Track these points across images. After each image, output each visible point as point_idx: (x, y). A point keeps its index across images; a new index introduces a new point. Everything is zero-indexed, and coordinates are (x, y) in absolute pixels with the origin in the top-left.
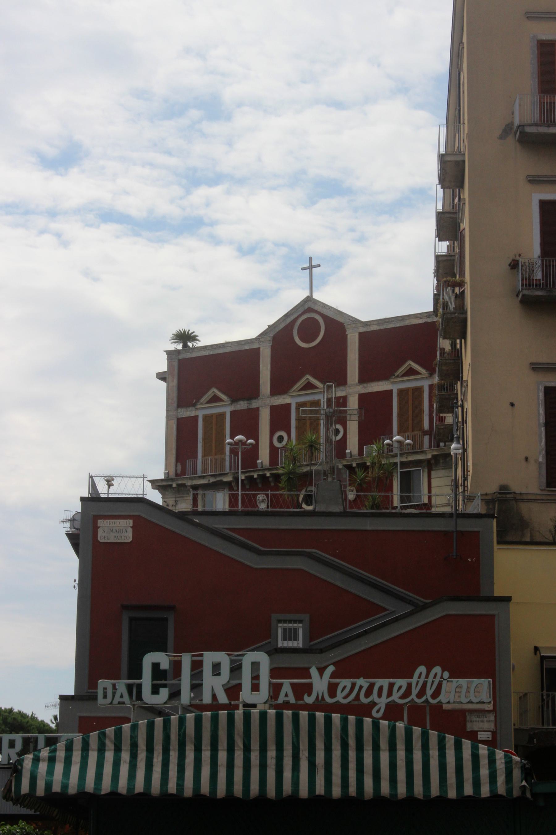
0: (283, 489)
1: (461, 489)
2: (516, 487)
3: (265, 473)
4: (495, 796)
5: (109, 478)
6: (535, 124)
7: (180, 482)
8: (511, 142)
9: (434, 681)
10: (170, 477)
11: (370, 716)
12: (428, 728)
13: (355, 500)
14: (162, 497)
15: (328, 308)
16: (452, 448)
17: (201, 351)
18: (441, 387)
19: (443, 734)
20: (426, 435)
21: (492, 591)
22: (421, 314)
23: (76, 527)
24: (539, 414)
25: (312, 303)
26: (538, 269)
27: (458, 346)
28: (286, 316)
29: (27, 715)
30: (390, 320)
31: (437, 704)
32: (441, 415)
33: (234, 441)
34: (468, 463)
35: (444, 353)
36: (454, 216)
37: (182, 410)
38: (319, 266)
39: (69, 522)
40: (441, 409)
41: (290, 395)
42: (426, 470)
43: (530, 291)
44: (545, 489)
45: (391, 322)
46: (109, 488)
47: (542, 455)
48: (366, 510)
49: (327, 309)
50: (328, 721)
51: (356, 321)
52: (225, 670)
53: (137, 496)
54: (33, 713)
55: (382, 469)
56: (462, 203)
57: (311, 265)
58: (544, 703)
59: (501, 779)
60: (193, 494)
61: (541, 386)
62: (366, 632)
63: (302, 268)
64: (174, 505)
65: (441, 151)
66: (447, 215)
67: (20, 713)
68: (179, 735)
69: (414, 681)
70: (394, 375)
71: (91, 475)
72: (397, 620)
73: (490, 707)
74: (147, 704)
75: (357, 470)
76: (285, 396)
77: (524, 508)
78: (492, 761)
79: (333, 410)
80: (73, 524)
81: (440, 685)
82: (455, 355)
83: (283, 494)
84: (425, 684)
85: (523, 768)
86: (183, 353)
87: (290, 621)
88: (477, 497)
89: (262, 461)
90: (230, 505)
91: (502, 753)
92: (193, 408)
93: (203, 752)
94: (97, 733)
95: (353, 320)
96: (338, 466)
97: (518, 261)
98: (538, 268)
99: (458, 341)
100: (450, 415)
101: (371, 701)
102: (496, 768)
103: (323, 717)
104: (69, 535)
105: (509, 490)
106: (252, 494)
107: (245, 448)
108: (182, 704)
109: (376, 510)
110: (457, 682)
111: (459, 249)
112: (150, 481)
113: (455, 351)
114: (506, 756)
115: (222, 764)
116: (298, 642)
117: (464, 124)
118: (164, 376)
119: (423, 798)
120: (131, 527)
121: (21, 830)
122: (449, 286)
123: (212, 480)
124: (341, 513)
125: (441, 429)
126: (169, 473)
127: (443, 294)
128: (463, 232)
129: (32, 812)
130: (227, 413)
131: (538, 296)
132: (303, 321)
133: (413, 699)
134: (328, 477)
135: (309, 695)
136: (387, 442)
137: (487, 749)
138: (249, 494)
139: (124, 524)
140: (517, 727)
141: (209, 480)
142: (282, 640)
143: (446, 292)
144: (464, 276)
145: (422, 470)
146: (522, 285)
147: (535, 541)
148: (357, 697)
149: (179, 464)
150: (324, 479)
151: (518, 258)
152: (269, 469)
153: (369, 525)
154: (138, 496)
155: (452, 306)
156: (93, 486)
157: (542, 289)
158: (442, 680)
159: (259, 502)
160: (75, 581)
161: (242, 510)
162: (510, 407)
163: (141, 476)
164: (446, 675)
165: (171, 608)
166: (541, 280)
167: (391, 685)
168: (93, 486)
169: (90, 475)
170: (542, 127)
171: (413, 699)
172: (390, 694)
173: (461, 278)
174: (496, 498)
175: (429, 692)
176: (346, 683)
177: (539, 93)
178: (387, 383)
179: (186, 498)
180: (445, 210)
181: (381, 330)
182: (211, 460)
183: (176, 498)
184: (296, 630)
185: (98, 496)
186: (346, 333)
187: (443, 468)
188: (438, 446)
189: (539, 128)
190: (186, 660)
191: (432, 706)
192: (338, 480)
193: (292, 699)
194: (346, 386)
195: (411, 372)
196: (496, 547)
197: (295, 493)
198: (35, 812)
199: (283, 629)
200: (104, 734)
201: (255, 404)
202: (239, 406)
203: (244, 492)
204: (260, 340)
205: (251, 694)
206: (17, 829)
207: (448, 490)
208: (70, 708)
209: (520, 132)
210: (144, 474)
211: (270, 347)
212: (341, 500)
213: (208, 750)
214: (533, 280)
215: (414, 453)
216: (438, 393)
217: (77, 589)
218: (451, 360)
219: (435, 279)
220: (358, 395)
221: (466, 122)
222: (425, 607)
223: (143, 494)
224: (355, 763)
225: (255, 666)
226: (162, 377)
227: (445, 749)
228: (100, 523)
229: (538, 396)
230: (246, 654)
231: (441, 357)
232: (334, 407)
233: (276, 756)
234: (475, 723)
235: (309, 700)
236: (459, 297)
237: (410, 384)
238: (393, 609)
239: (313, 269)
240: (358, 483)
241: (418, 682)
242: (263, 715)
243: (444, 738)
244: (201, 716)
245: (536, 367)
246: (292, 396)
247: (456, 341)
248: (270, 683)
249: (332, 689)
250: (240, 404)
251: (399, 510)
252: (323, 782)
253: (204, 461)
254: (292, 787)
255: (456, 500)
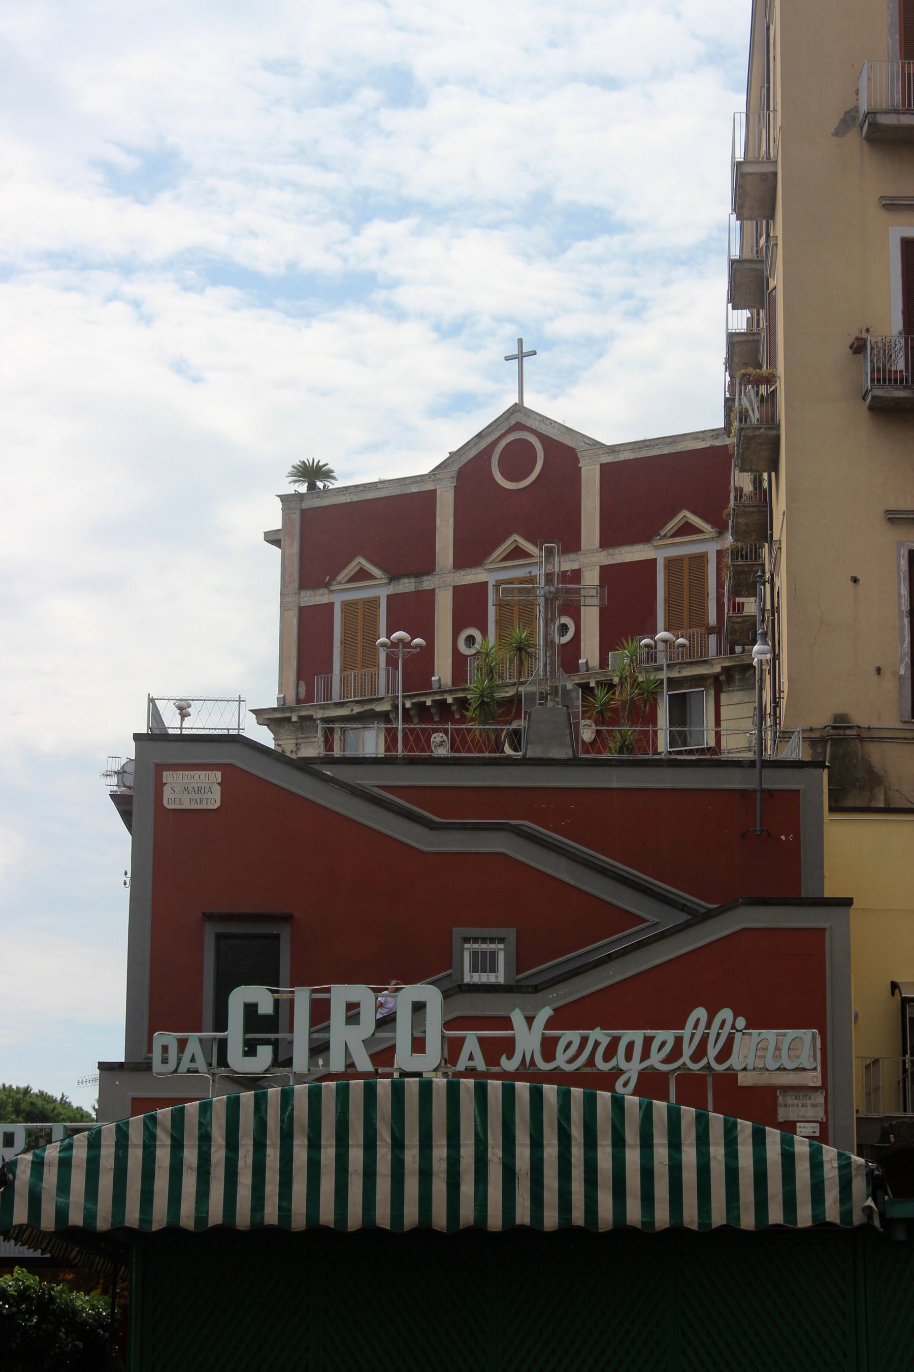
0: (472, 720)
1: (769, 721)
2: (861, 718)
3: (445, 697)
4: (821, 1226)
5: (183, 702)
6: (895, 110)
7: (304, 713)
8: (854, 139)
9: (721, 1032)
10: (287, 705)
11: (611, 1089)
12: (710, 1106)
13: (593, 743)
16: (755, 652)
17: (339, 495)
18: (736, 553)
19: (732, 1119)
20: (711, 634)
21: (822, 890)
23: (128, 784)
24: (900, 596)
25: (522, 415)
26: (899, 353)
27: (765, 484)
29: (54, 1098)
30: (652, 443)
31: (725, 1072)
32: (737, 600)
33: (391, 641)
34: (781, 678)
35: (741, 497)
36: (758, 266)
37: (306, 593)
38: (534, 353)
39: (116, 776)
40: (736, 591)
41: (486, 568)
42: (712, 692)
43: (884, 390)
44: (910, 721)
46: (182, 720)
47: (904, 665)
48: (610, 755)
49: (547, 425)
50: (537, 1096)
51: (596, 444)
52: (368, 1018)
53: (228, 732)
54: (64, 1095)
55: (637, 687)
56: (771, 243)
57: (520, 352)
58: (908, 1076)
59: (832, 1195)
60: (324, 729)
61: (902, 549)
62: (610, 958)
63: (505, 357)
64: (294, 751)
65: (736, 157)
66: (747, 266)
67: (42, 1095)
68: (282, 1121)
69: (686, 1033)
70: (660, 535)
71: (152, 697)
72: (662, 936)
73: (814, 1079)
74: (237, 1073)
75: (596, 691)
76: (479, 570)
77: (876, 754)
78: (816, 1165)
79: (556, 588)
80: (122, 780)
81: (730, 1040)
82: (760, 499)
83: (473, 728)
84: (704, 1039)
85: (870, 1175)
86: (309, 499)
87: (484, 940)
88: (796, 733)
89: (440, 678)
90: (387, 749)
91: (833, 1151)
92: (326, 591)
93: (323, 1150)
94: (141, 1117)
96: (564, 687)
97: (865, 340)
98: (898, 352)
99: (765, 475)
100: (752, 599)
101: (614, 1067)
102: (823, 1176)
103: (529, 1089)
104: (113, 796)
105: (849, 723)
106: (419, 728)
107: (409, 652)
108: (295, 1073)
109: (627, 756)
110: (759, 1035)
111: (766, 322)
112: (253, 711)
113: (760, 493)
114: (840, 1155)
115: (355, 1171)
116: (498, 974)
117: (775, 110)
118: (277, 537)
119: (699, 1228)
120: (218, 783)
121: (16, 1283)
122: (749, 382)
123: (357, 709)
124: (569, 759)
125: (738, 623)
126: (286, 698)
127: (740, 399)
128: (774, 292)
129: (38, 1254)
131: (899, 398)
132: (507, 445)
133: (684, 1064)
134: (547, 701)
135: (510, 1057)
136: (646, 641)
137: (808, 1143)
138: (416, 728)
139: (207, 778)
140: (861, 1115)
141: (352, 710)
142: (470, 972)
143: (745, 392)
144: (775, 367)
145: (705, 692)
146: (872, 380)
147: (892, 806)
148: (591, 1061)
149: (302, 683)
150: (541, 704)
151: (864, 335)
152: (450, 692)
153: (615, 780)
154: (230, 732)
155: (755, 417)
156: (155, 714)
157: (905, 387)
158: (735, 1031)
159: (435, 746)
160: (126, 873)
161: (403, 755)
162: (853, 584)
163: (235, 699)
164: (741, 1022)
165: (286, 918)
166: (904, 372)
167: (648, 1041)
168: (155, 714)
169: (151, 697)
170: (906, 116)
171: (684, 1064)
172: (645, 1055)
173: (770, 369)
174: (828, 736)
175: (712, 1051)
176: (572, 1036)
177: (901, 59)
178: (646, 547)
180: (744, 258)
181: (636, 459)
182: (355, 676)
183: (297, 739)
184: (493, 954)
185: (163, 732)
187: (740, 688)
188: (732, 651)
189: (901, 116)
190: (302, 997)
191: (717, 1076)
192: (565, 706)
193: (480, 1064)
194: (580, 553)
195: (687, 529)
196: (827, 816)
197: (493, 727)
198: (42, 1254)
199: (471, 952)
200: (153, 1119)
201: (427, 583)
202: (401, 586)
203: (406, 726)
204: (435, 477)
205: (412, 1055)
206: (10, 1281)
207: (748, 724)
208: (117, 1083)
209: (870, 124)
210: (240, 696)
211: (453, 488)
212: (568, 738)
213: (331, 1146)
214: (890, 371)
215: (691, 664)
216: (732, 562)
217: (130, 887)
218: (753, 506)
219: (727, 374)
220: (599, 567)
221: (779, 108)
222: (708, 915)
223: (239, 729)
224: (583, 1168)
225: (419, 1007)
226: (273, 538)
227: (736, 1144)
228: (168, 777)
229: (899, 565)
230: (403, 988)
231: (735, 502)
232: (557, 585)
233: (448, 1157)
234: (791, 1108)
235: (509, 1065)
236: (767, 402)
237: (686, 548)
238: (657, 920)
239: (524, 358)
240: (597, 710)
241: (693, 1035)
242: (426, 1088)
243: (735, 1125)
244: (320, 1088)
245: (895, 518)
246: (490, 570)
247: (761, 475)
248: (443, 1037)
249: (549, 1047)
250: (404, 584)
251: (665, 755)
252: (528, 1203)
254: (475, 1210)
255: (761, 741)
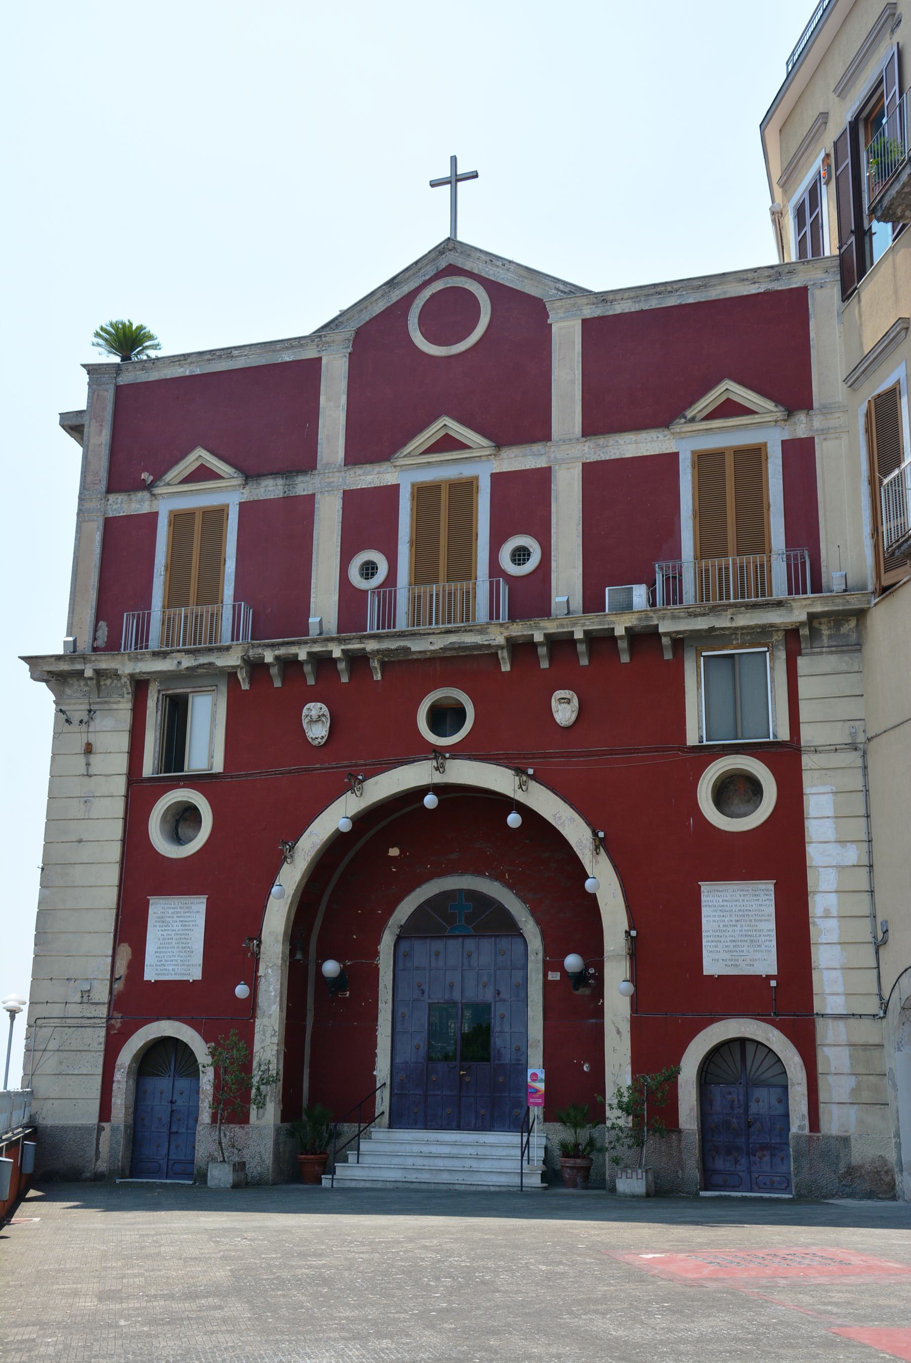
3: (329, 649)
14: (54, 701)
15: (500, 264)
22: (755, 270)
28: (392, 283)
41: (398, 464)
42: (782, 655)
45: (671, 292)
51: (574, 291)
70: (685, 418)
76: (385, 466)
92: (146, 494)
95: (567, 290)
130: (231, 508)
141: (179, 663)
152: (340, 641)
178: (661, 437)
179: (115, 706)
186: (549, 322)
239: (459, 184)
250: (266, 486)
253: (169, 619)
